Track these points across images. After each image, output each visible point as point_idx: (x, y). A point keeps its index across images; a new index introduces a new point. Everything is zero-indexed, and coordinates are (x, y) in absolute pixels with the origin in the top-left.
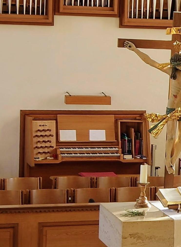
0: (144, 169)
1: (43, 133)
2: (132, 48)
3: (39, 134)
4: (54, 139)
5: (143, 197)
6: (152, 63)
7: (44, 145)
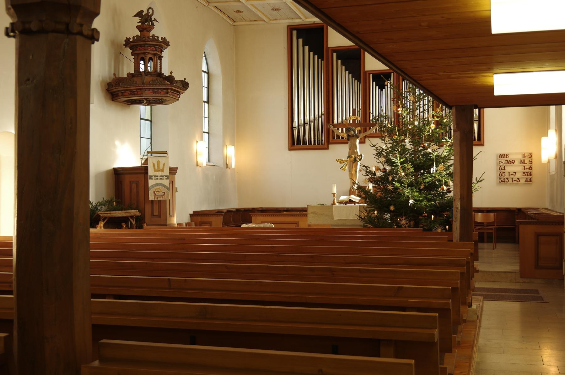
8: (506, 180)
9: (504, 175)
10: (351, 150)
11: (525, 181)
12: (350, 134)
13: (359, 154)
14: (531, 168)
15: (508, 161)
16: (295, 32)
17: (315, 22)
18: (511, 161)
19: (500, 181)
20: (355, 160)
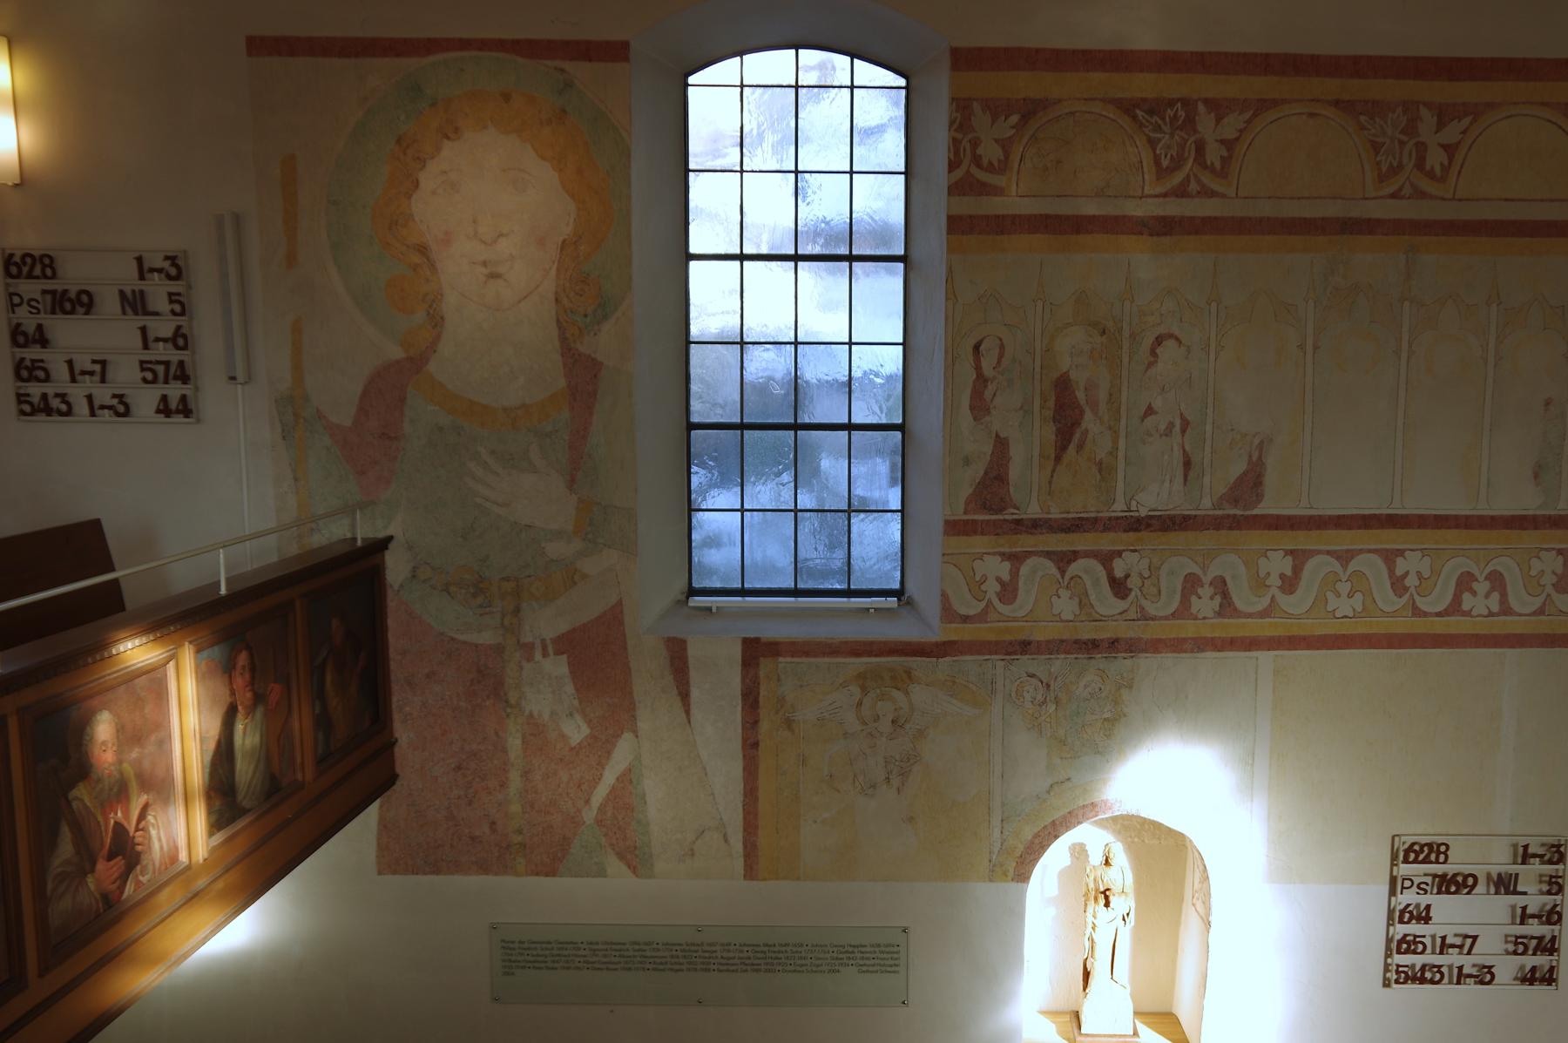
8: (55, 403)
9: (41, 374)
11: (158, 411)
14: (181, 342)
15: (58, 296)
18: (73, 295)
19: (27, 408)
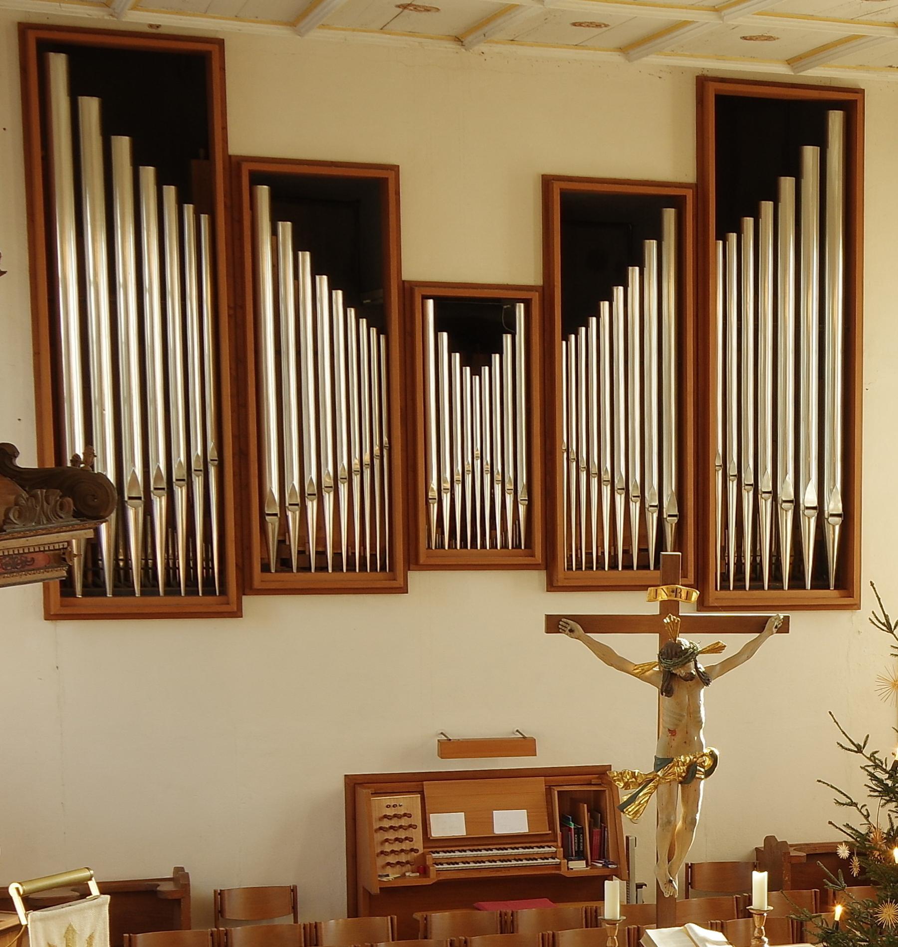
0: (613, 890)
1: (395, 823)
2: (576, 633)
3: (386, 824)
4: (417, 834)
5: (760, 938)
6: (620, 664)
7: (397, 847)
10: (678, 737)
12: (682, 672)
13: (706, 751)
16: (58, 65)
17: (158, 27)
20: (690, 777)
